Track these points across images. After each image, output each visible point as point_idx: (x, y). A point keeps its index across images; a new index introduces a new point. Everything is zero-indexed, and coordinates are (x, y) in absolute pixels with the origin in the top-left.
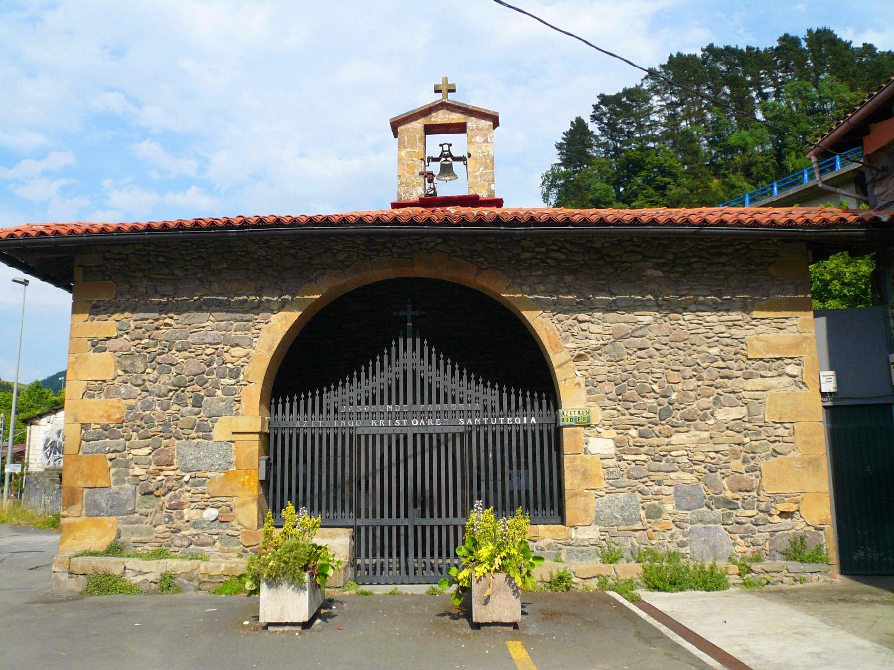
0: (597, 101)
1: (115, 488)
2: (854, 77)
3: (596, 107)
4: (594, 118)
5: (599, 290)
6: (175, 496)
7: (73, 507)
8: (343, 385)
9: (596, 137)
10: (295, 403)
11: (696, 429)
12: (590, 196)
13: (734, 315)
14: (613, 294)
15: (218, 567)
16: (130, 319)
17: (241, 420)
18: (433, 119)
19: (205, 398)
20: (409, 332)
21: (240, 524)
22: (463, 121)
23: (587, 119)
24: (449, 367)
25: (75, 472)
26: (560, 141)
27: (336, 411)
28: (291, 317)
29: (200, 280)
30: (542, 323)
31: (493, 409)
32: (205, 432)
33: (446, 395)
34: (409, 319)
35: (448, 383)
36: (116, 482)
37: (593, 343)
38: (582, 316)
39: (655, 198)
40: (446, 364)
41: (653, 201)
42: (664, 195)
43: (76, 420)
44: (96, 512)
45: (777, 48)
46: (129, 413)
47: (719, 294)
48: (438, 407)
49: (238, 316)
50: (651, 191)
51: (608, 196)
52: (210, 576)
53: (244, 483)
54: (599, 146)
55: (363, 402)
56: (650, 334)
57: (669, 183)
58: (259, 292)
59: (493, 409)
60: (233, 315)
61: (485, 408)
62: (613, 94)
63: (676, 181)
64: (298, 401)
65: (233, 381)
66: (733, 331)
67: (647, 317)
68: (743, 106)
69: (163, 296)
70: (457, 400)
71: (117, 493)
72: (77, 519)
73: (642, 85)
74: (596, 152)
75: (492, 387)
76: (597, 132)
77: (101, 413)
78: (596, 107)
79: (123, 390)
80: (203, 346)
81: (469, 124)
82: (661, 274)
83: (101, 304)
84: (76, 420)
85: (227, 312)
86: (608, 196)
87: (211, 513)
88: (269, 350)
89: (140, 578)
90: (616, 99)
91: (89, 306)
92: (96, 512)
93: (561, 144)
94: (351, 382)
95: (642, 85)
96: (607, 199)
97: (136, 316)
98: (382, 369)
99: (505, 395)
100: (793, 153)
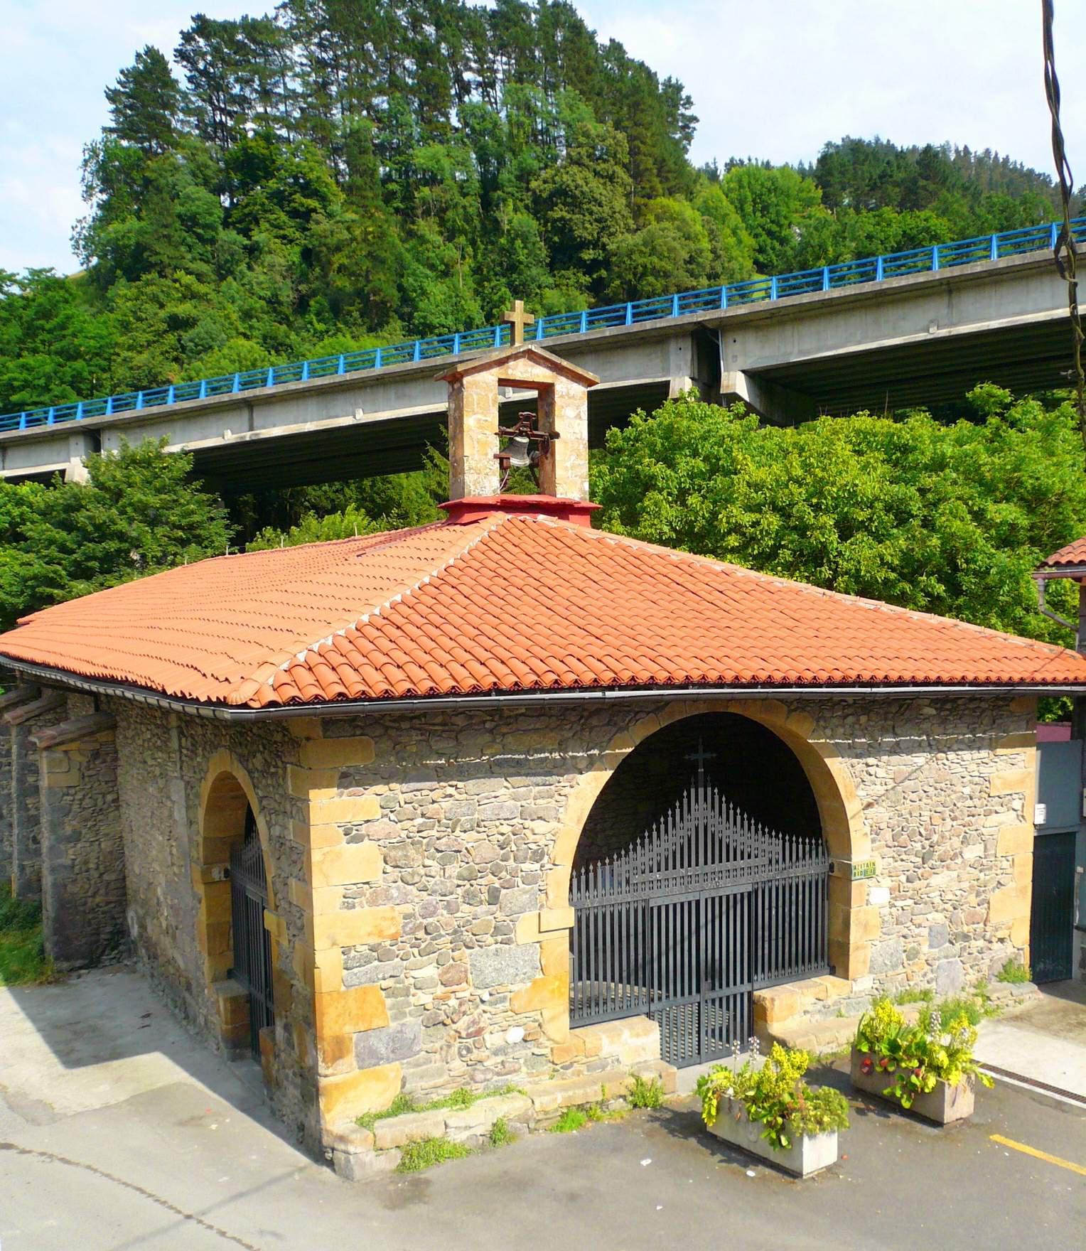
0: (189, 25)
1: (394, 1025)
2: (599, 94)
3: (187, 37)
4: (181, 55)
5: (884, 731)
6: (474, 1022)
7: (340, 1062)
8: (635, 850)
9: (185, 95)
10: (583, 877)
11: (948, 868)
12: (179, 209)
13: (984, 753)
14: (896, 735)
15: (555, 1100)
16: (398, 791)
17: (547, 915)
18: (510, 371)
19: (503, 891)
20: (701, 778)
21: (549, 1039)
22: (549, 381)
23: (169, 56)
24: (746, 822)
25: (339, 1016)
26: (115, 85)
27: (628, 882)
28: (602, 777)
29: (491, 731)
30: (837, 766)
31: (777, 862)
32: (503, 933)
33: (742, 853)
34: (701, 764)
35: (736, 837)
36: (395, 1018)
37: (880, 790)
38: (871, 761)
39: (289, 232)
40: (750, 825)
41: (284, 237)
42: (305, 229)
43: (334, 944)
44: (373, 1062)
45: (493, 11)
46: (406, 924)
47: (973, 732)
48: (730, 865)
49: (539, 779)
50: (284, 217)
51: (211, 214)
52: (546, 1113)
53: (553, 991)
54: (187, 111)
55: (655, 869)
56: (922, 777)
57: (314, 210)
58: (562, 747)
59: (777, 862)
60: (534, 779)
61: (770, 861)
62: (220, 19)
63: (325, 207)
64: (587, 872)
65: (537, 866)
66: (982, 769)
67: (920, 759)
68: (432, 94)
69: (440, 756)
70: (746, 856)
71: (401, 1032)
72: (347, 1076)
73: (276, 18)
74: (182, 121)
75: (777, 836)
76: (184, 85)
77: (369, 929)
78: (187, 37)
79: (395, 893)
80: (497, 823)
81: (558, 388)
82: (934, 712)
83: (351, 771)
84: (334, 944)
85: (527, 775)
86: (211, 214)
87: (516, 1035)
88: (579, 821)
89: (464, 1135)
90: (227, 29)
91: (337, 775)
92: (373, 1062)
93: (116, 92)
94: (643, 845)
95: (276, 18)
96: (209, 219)
97: (405, 787)
98: (674, 825)
99: (787, 844)
100: (510, 202)
